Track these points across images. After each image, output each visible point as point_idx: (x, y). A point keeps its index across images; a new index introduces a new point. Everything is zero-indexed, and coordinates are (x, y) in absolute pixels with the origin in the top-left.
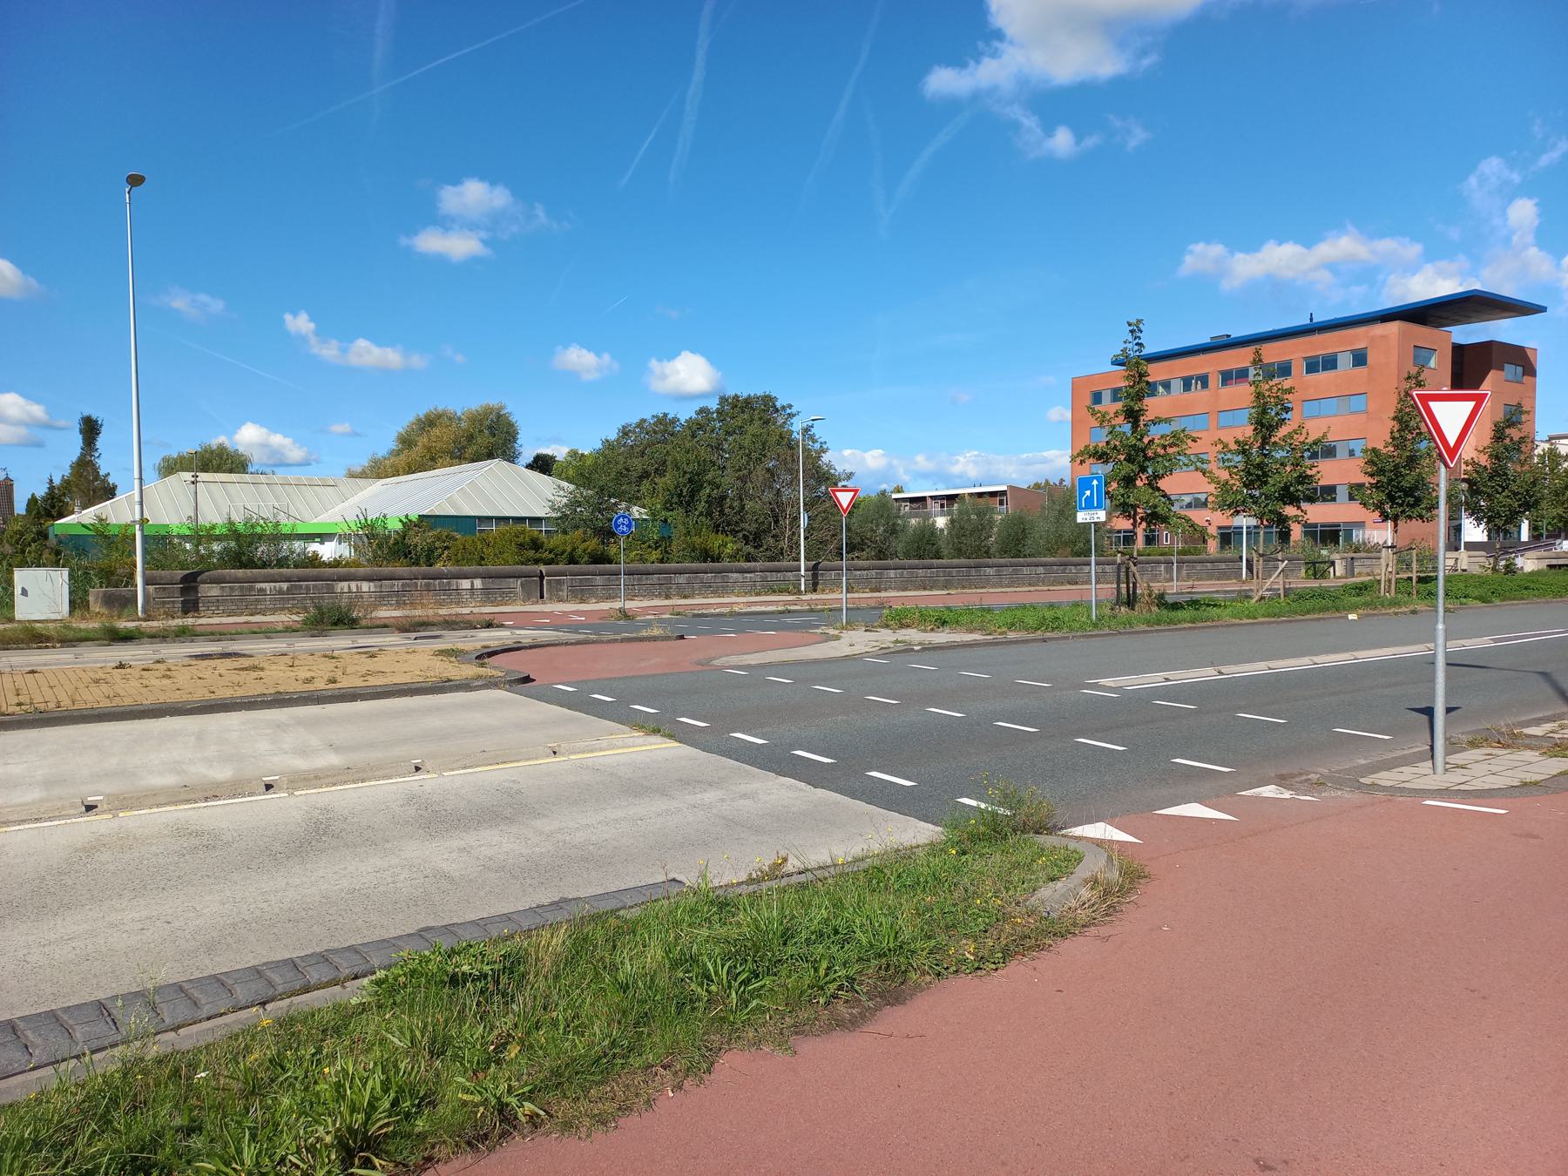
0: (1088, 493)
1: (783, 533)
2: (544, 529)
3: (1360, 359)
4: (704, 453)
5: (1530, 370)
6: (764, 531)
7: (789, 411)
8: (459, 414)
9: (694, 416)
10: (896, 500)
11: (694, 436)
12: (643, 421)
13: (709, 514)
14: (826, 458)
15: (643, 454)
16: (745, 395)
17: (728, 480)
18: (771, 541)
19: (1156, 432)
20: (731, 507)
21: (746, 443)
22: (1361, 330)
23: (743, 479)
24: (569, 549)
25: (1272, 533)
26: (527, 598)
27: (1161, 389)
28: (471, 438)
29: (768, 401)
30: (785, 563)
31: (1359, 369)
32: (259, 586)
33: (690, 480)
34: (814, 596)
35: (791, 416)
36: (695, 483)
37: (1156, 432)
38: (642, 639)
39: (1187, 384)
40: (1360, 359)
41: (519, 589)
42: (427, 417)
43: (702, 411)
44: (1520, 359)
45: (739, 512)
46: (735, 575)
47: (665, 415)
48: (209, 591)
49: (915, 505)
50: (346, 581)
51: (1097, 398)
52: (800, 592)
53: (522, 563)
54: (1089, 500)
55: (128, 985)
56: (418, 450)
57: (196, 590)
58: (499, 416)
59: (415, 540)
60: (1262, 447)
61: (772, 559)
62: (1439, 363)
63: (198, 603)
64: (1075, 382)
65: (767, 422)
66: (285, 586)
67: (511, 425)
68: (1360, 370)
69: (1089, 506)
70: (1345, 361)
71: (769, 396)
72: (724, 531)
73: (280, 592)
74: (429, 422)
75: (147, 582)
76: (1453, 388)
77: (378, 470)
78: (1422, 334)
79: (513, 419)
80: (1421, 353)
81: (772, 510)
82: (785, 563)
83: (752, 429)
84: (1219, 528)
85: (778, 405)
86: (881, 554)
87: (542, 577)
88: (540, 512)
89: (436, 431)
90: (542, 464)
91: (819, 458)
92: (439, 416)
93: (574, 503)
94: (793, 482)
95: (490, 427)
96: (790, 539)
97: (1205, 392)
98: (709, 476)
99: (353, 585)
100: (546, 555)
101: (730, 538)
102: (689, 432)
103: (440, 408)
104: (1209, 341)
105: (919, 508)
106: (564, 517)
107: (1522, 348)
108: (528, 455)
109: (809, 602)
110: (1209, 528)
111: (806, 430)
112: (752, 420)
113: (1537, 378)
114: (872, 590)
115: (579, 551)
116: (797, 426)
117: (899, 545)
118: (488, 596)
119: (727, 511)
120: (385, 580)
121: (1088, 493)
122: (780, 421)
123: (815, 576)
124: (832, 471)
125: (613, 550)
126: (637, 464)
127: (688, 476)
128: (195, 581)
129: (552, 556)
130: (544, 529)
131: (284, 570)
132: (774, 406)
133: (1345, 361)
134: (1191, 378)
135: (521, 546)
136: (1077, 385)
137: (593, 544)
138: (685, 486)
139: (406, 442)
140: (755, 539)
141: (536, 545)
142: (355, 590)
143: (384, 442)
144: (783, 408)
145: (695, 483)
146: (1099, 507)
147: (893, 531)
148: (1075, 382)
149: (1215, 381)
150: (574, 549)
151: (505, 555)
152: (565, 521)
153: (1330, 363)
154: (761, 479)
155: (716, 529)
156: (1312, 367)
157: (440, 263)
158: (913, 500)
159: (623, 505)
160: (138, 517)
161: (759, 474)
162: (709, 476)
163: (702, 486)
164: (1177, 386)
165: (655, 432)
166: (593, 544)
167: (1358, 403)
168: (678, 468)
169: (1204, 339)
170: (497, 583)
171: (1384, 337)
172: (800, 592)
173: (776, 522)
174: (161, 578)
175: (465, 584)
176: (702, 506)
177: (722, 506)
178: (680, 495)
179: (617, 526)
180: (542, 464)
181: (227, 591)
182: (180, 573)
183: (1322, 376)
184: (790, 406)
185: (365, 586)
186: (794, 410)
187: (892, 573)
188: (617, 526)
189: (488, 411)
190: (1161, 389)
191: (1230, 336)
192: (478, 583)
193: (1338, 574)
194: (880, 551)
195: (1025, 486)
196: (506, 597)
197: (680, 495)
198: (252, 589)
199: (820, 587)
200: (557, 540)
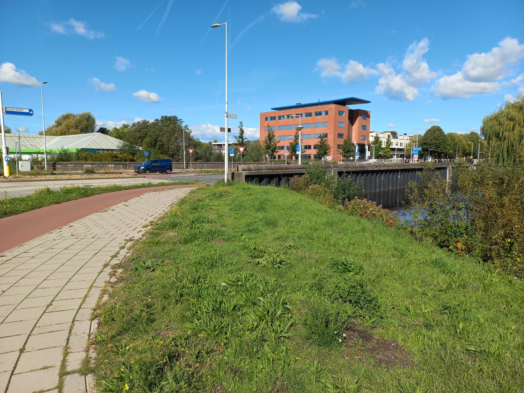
1: (180, 155)
3: (327, 113)
4: (157, 132)
5: (369, 116)
6: (175, 154)
8: (75, 114)
9: (154, 121)
10: (213, 145)
11: (154, 127)
12: (139, 122)
13: (159, 149)
14: (191, 134)
15: (140, 131)
16: (168, 116)
17: (165, 140)
18: (177, 157)
19: (245, 140)
20: (166, 147)
21: (169, 130)
22: (327, 106)
23: (169, 140)
24: (124, 158)
25: (395, 154)
26: (123, 169)
27: (282, 118)
29: (175, 118)
30: (181, 162)
32: (68, 165)
33: (154, 140)
34: (187, 170)
35: (182, 122)
36: (156, 141)
37: (245, 140)
38: (156, 174)
40: (327, 113)
41: (122, 167)
43: (156, 120)
44: (366, 114)
45: (168, 149)
47: (145, 120)
48: (58, 166)
49: (219, 147)
50: (110, 164)
51: (267, 119)
52: (184, 169)
53: (113, 161)
56: (63, 126)
57: (55, 166)
60: (270, 142)
61: (177, 161)
62: (345, 115)
65: (175, 124)
66: (73, 165)
68: (327, 116)
69: (232, 153)
70: (323, 113)
71: (175, 116)
72: (164, 154)
73: (72, 167)
74: (67, 117)
75: (47, 164)
77: (50, 132)
78: (341, 108)
80: (340, 113)
81: (177, 148)
82: (181, 162)
83: (171, 126)
85: (178, 119)
86: (208, 161)
87: (126, 164)
88: (116, 148)
91: (189, 134)
92: (69, 115)
93: (124, 146)
94: (182, 141)
95: (86, 119)
96: (182, 156)
98: (159, 139)
99: (87, 165)
100: (119, 159)
101: (166, 156)
102: (152, 126)
103: (70, 113)
104: (296, 105)
105: (220, 147)
106: (121, 150)
108: (98, 128)
109: (186, 171)
111: (186, 126)
112: (171, 124)
113: (371, 119)
114: (200, 169)
115: (127, 159)
116: (183, 125)
117: (213, 158)
118: (115, 168)
119: (164, 148)
122: (179, 124)
123: (187, 165)
124: (193, 138)
125: (135, 158)
126: (139, 134)
127: (154, 139)
129: (120, 160)
131: (73, 162)
132: (177, 119)
133: (323, 113)
135: (112, 157)
136: (262, 115)
137: (131, 157)
138: (153, 142)
139: (59, 123)
140: (172, 156)
141: (116, 157)
144: (179, 120)
145: (156, 141)
147: (211, 154)
150: (126, 158)
151: (108, 159)
153: (320, 114)
154: (174, 140)
155: (162, 153)
158: (218, 145)
159: (137, 147)
160: (45, 151)
161: (173, 138)
162: (159, 139)
163: (157, 142)
164: (286, 117)
165: (143, 125)
166: (131, 157)
167: (326, 124)
168: (151, 137)
169: (294, 104)
170: (117, 166)
172: (184, 169)
173: (178, 151)
175: (110, 166)
176: (158, 147)
177: (163, 147)
178: (152, 144)
179: (145, 154)
181: (62, 166)
182: (52, 162)
183: (319, 117)
184: (181, 119)
185: (90, 166)
186: (182, 121)
187: (205, 165)
188: (145, 154)
190: (282, 118)
191: (300, 104)
192: (113, 165)
194: (207, 160)
195: (451, 76)
196: (119, 168)
197: (152, 144)
198: (67, 166)
199: (188, 168)
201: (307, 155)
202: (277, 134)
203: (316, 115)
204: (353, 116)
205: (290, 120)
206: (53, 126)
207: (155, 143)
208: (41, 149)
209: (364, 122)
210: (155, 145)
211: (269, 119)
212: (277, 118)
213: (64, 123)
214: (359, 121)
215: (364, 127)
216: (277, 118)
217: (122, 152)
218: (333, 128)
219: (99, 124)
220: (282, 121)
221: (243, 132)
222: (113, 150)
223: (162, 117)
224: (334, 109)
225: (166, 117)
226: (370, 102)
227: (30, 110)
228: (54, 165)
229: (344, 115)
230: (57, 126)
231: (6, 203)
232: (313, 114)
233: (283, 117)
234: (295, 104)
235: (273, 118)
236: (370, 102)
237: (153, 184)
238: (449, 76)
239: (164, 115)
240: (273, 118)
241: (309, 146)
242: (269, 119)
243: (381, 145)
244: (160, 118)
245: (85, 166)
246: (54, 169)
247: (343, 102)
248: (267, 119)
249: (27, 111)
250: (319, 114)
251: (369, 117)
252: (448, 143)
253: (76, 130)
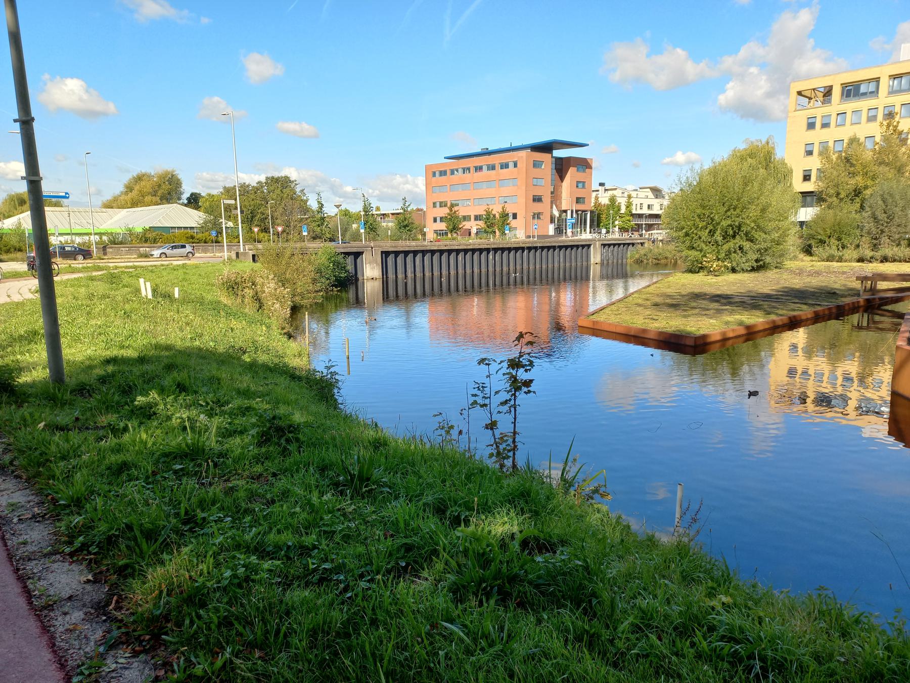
22: (515, 153)
28: (160, 186)
35: (296, 184)
39: (464, 170)
42: (138, 176)
43: (259, 182)
44: (584, 164)
48: (109, 250)
51: (434, 174)
55: (8, 564)
56: (135, 193)
58: (173, 176)
59: (148, 235)
64: (426, 167)
67: (179, 180)
70: (511, 165)
74: (139, 178)
79: (179, 177)
89: (143, 183)
90: (194, 201)
93: (205, 223)
103: (143, 171)
106: (202, 227)
107: (585, 159)
111: (302, 191)
116: (298, 189)
133: (511, 165)
135: (187, 238)
139: (129, 188)
141: (192, 237)
143: (117, 188)
148: (426, 167)
152: (203, 228)
157: (64, 500)
164: (460, 171)
180: (194, 201)
183: (505, 170)
189: (167, 173)
200: (200, 236)
204: (561, 167)
205: (467, 175)
206: (122, 193)
207: (252, 217)
208: (101, 227)
209: (580, 176)
210: (252, 219)
211: (437, 174)
212: (448, 172)
213: (137, 188)
214: (572, 174)
215: (581, 184)
216: (448, 172)
217: (204, 230)
218: (524, 188)
219: (187, 190)
221: (322, 205)
222: (193, 228)
223: (267, 178)
224: (525, 158)
225: (273, 178)
227: (66, 193)
228: (104, 248)
229: (543, 167)
230: (126, 193)
232: (498, 167)
233: (457, 171)
235: (443, 173)
237: (572, 304)
239: (270, 175)
240: (443, 173)
242: (437, 174)
243: (619, 210)
244: (263, 180)
245: (141, 249)
246: (105, 254)
247: (546, 148)
248: (434, 174)
249: (64, 194)
250: (505, 166)
251: (591, 168)
253: (154, 198)
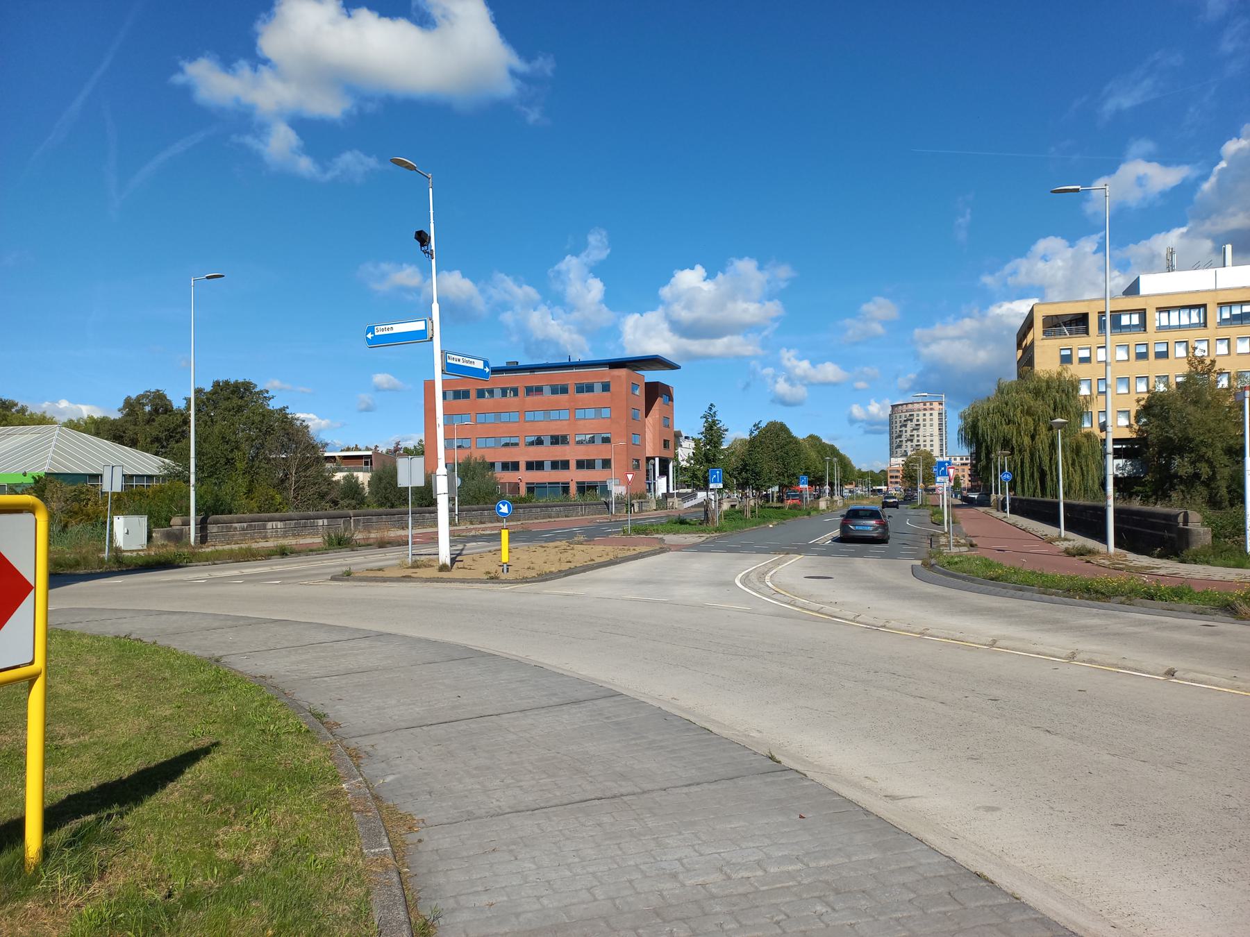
0: (715, 476)
2: (134, 484)
7: (266, 395)
27: (487, 394)
29: (247, 386)
31: (605, 393)
39: (504, 393)
40: (606, 387)
46: (427, 515)
54: (715, 479)
62: (641, 392)
63: (207, 537)
66: (245, 525)
70: (598, 387)
76: (1116, 478)
84: (527, 483)
97: (516, 399)
104: (505, 365)
110: (521, 484)
120: (288, 520)
121: (715, 476)
128: (206, 523)
130: (134, 484)
133: (598, 387)
134: (507, 388)
142: (274, 527)
146: (720, 482)
149: (522, 392)
156: (580, 389)
164: (498, 393)
171: (619, 377)
174: (244, 519)
183: (585, 395)
184: (267, 392)
186: (270, 394)
190: (487, 394)
191: (517, 363)
193: (636, 511)
201: (558, 483)
202: (724, 420)
203: (554, 391)
216: (473, 394)
220: (487, 401)
223: (216, 384)
225: (227, 383)
226: (223, 276)
231: (400, 504)
233: (491, 392)
234: (503, 364)
236: (223, 276)
238: (493, 22)
239: (222, 378)
241: (537, 462)
252: (352, 747)
